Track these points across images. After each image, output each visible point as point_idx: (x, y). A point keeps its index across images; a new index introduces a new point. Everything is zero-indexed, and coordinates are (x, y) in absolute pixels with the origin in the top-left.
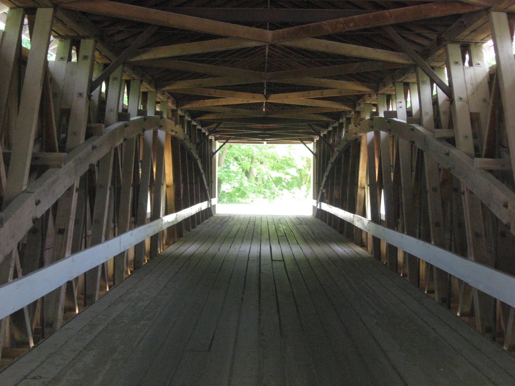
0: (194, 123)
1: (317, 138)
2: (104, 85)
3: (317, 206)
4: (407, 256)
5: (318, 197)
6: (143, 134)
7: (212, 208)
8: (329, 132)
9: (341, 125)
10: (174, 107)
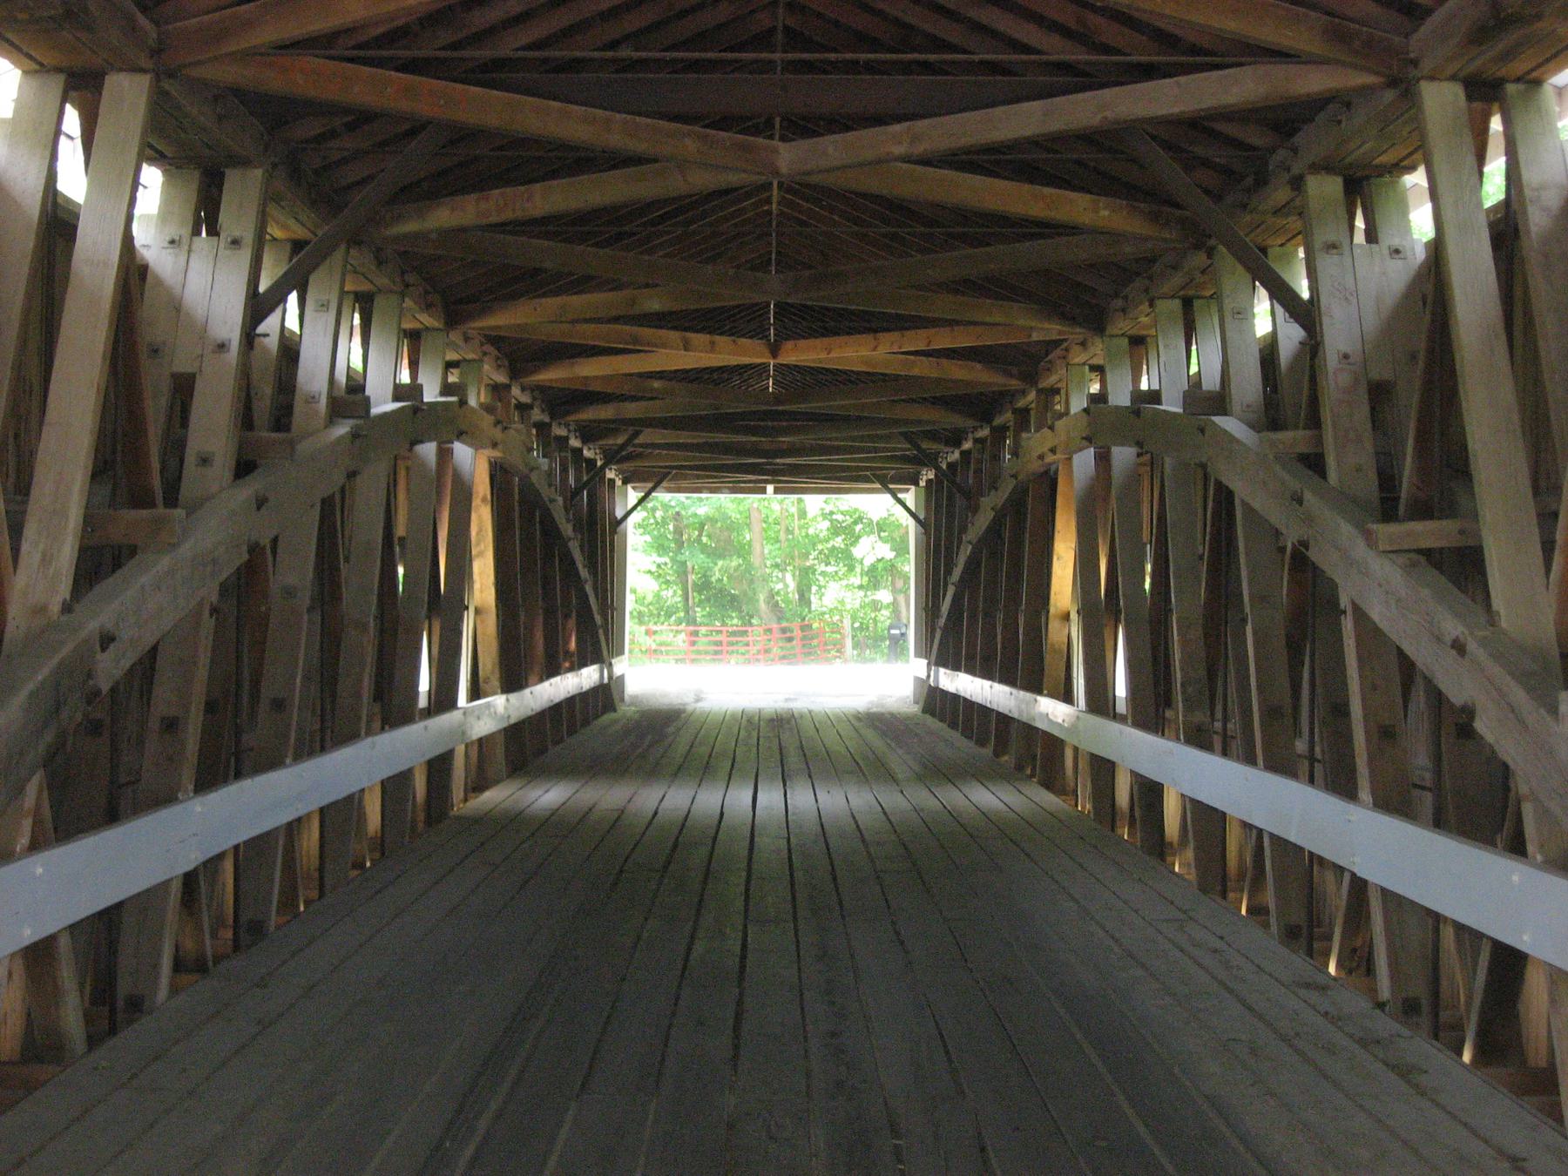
0: (559, 431)
1: (928, 475)
2: (293, 298)
3: (929, 676)
4: (1188, 806)
5: (931, 648)
6: (408, 454)
7: (613, 686)
8: (966, 455)
9: (1000, 433)
10: (501, 378)
